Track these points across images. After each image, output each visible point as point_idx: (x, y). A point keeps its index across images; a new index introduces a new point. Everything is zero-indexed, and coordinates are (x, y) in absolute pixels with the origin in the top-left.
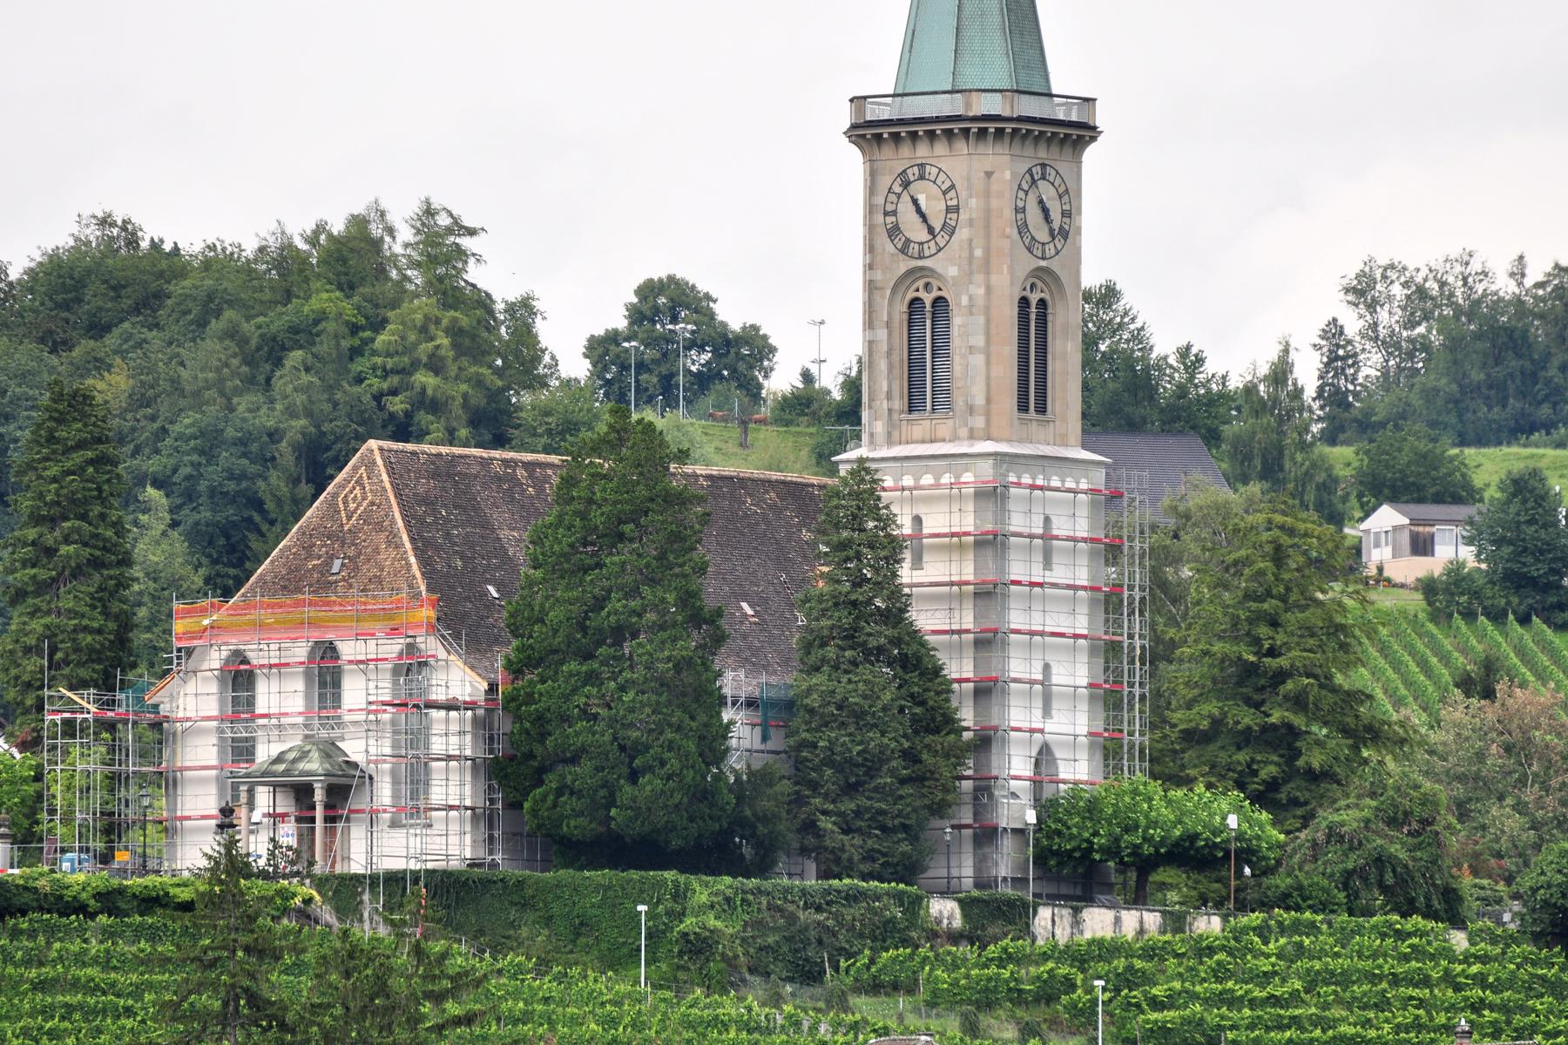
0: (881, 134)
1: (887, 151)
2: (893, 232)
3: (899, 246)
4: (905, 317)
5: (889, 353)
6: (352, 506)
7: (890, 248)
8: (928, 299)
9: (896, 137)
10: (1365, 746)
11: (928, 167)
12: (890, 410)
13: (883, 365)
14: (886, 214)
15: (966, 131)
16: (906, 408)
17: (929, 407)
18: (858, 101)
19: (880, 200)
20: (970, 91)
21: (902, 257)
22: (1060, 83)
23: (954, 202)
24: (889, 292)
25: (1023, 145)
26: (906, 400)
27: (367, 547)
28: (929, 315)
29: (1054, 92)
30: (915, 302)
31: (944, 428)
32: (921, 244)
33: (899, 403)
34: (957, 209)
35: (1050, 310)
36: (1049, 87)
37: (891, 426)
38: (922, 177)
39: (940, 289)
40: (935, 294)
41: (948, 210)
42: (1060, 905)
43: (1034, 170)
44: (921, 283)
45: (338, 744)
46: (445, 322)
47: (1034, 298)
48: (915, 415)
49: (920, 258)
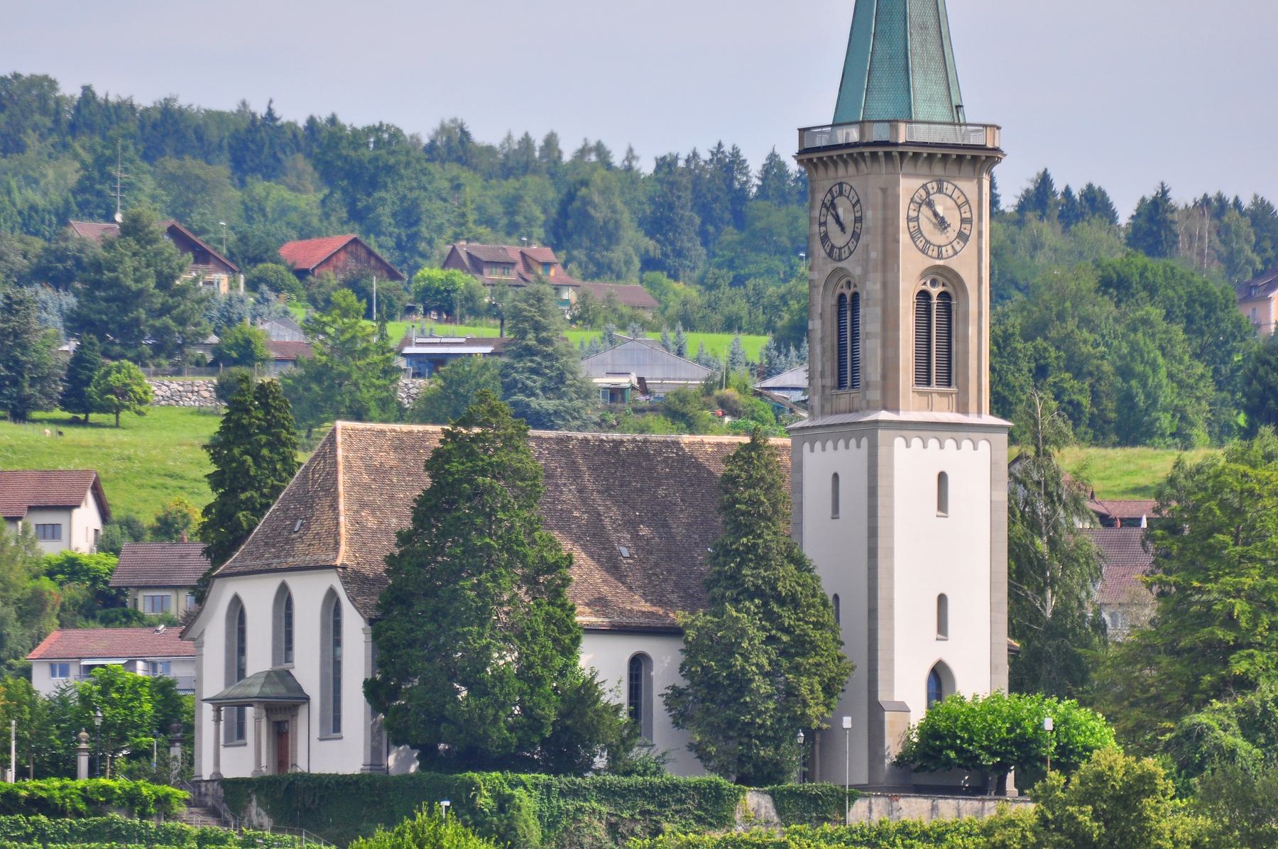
0: (877, 153)
4: (835, 309)
5: (822, 340)
8: (848, 293)
9: (874, 155)
12: (823, 387)
14: (821, 224)
15: (945, 157)
16: (836, 385)
17: (849, 383)
18: (802, 131)
22: (971, 114)
24: (821, 289)
25: (916, 166)
26: (836, 378)
30: (842, 296)
33: (830, 381)
35: (954, 302)
38: (841, 194)
40: (853, 290)
42: (876, 796)
46: (180, 328)
47: (935, 291)
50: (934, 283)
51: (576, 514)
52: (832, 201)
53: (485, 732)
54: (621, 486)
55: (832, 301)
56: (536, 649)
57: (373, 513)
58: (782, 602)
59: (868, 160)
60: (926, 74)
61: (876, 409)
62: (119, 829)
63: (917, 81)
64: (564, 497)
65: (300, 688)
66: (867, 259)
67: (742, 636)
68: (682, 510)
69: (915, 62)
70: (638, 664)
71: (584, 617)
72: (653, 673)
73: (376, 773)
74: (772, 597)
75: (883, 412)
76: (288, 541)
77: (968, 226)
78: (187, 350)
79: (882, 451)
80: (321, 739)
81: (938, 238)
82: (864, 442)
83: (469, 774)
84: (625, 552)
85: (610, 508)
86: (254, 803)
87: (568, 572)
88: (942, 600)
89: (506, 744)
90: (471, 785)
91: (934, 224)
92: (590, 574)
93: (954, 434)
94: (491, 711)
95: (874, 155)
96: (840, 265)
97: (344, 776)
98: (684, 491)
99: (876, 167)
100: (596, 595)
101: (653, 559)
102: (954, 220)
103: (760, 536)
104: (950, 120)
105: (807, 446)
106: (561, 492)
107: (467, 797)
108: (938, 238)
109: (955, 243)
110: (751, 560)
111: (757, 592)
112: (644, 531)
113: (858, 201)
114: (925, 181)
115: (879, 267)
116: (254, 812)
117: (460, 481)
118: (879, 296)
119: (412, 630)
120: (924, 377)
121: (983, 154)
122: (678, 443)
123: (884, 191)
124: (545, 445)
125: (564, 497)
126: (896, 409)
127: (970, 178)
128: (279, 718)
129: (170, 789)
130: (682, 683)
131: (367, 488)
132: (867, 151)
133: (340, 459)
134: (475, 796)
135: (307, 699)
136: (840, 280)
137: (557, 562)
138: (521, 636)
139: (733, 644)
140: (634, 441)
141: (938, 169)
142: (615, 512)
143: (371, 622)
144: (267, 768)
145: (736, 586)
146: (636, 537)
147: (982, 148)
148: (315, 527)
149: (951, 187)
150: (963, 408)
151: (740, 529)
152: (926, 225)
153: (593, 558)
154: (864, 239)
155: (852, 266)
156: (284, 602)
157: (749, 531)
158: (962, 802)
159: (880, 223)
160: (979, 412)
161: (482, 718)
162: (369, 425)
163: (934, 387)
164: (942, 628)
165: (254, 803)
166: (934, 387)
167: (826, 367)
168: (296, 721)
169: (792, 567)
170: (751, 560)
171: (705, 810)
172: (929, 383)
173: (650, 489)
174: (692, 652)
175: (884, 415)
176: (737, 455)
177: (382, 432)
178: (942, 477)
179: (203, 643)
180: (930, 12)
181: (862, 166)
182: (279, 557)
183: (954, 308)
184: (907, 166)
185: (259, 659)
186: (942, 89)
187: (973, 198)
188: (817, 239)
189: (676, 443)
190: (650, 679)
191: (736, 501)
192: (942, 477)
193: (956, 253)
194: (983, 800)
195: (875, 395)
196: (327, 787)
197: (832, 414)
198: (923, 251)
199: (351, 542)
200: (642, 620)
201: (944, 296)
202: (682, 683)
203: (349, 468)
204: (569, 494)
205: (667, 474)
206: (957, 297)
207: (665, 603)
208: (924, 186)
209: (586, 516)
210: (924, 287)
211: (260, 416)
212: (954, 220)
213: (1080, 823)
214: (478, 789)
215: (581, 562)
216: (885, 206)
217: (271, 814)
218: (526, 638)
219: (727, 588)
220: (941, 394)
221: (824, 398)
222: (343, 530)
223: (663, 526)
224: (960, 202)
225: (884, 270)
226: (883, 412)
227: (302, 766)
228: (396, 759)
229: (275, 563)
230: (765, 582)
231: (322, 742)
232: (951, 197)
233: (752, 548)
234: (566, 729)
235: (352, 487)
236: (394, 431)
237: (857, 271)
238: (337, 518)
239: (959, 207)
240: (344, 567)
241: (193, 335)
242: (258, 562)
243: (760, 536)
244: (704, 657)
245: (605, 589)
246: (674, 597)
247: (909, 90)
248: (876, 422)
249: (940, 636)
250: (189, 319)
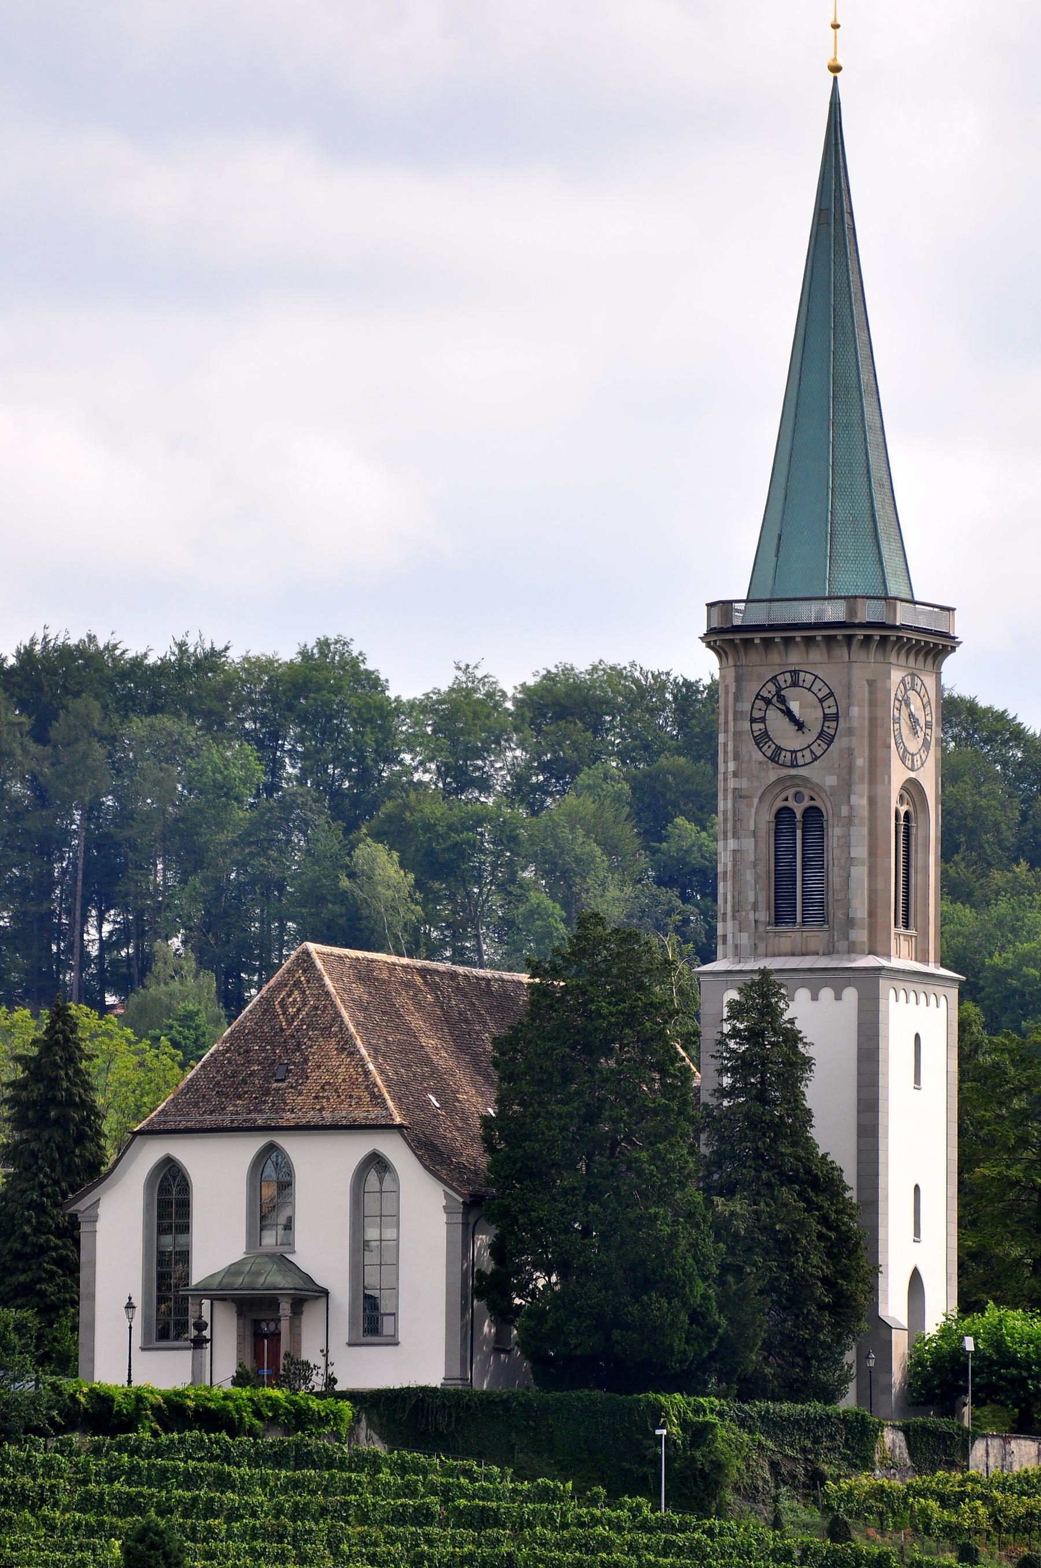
1: (754, 657)
2: (762, 739)
3: (769, 754)
5: (755, 864)
6: (292, 1010)
7: (758, 756)
8: (799, 809)
11: (802, 674)
13: (749, 876)
14: (753, 720)
16: (773, 921)
17: (799, 919)
19: (746, 706)
20: (855, 597)
21: (771, 764)
23: (833, 710)
24: (756, 801)
26: (773, 911)
27: (314, 1054)
28: (799, 825)
29: (917, 599)
31: (816, 937)
32: (794, 752)
34: (836, 717)
36: (887, 593)
37: (757, 938)
38: (795, 684)
39: (812, 799)
40: (807, 803)
41: (826, 718)
43: (780, 678)
44: (790, 793)
45: (287, 1256)
48: (783, 928)
49: (794, 765)
55: (768, 816)
62: (310, 1452)
66: (850, 768)
75: (870, 957)
80: (143, 1349)
88: (917, 1188)
95: (868, 638)
109: (814, 747)
115: (866, 779)
118: (866, 813)
123: (871, 683)
126: (888, 955)
149: (809, 678)
154: (840, 743)
167: (760, 897)
168: (300, 1319)
171: (851, 1449)
179: (97, 1216)
195: (860, 935)
197: (766, 956)
206: (916, 818)
210: (786, 804)
221: (757, 937)
231: (352, 1348)
232: (809, 689)
247: (881, 564)
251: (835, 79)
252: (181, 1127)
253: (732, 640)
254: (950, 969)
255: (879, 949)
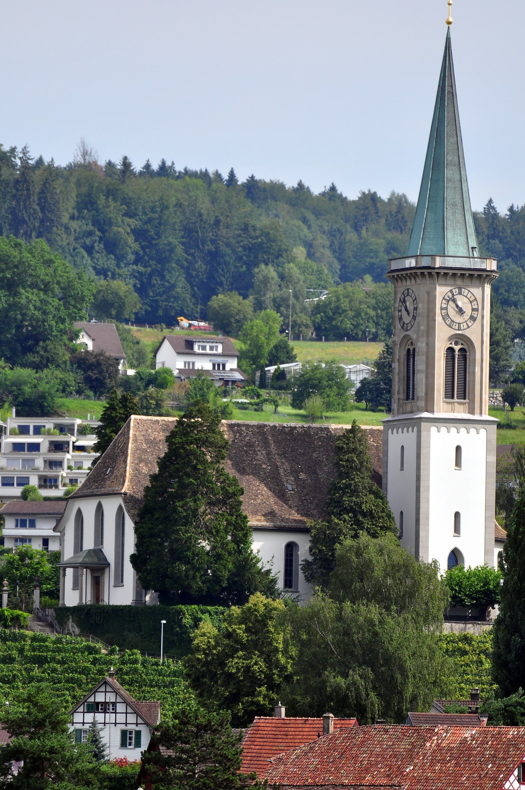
4: (405, 357)
5: (399, 373)
8: (411, 348)
10: (141, 264)
12: (399, 399)
25: (446, 279)
33: (402, 396)
35: (468, 354)
38: (408, 295)
40: (413, 347)
47: (457, 348)
50: (456, 343)
51: (264, 466)
52: (404, 299)
53: (188, 584)
54: (292, 452)
55: (404, 353)
56: (218, 539)
57: (146, 465)
58: (365, 515)
59: (420, 277)
60: (454, 230)
61: (422, 411)
63: (449, 234)
64: (258, 457)
65: (106, 559)
66: (419, 330)
67: (340, 533)
68: (325, 466)
69: (448, 224)
70: (290, 548)
71: (253, 522)
72: (299, 553)
73: (139, 605)
74: (360, 512)
76: (104, 480)
77: (476, 313)
78: (500, 375)
79: (423, 434)
80: (115, 586)
81: (458, 319)
82: (415, 429)
83: (180, 606)
84: (290, 487)
85: (284, 464)
86: (71, 620)
87: (241, 498)
88: (457, 515)
89: (200, 590)
90: (181, 611)
91: (456, 312)
92: (268, 499)
93: (466, 425)
94: (191, 572)
96: (407, 333)
97: (116, 606)
98: (329, 455)
99: (424, 281)
100: (270, 511)
101: (305, 491)
102: (468, 310)
103: (353, 479)
104: (467, 255)
105: (390, 431)
106: (257, 455)
107: (178, 619)
108: (458, 319)
109: (468, 322)
110: (348, 493)
111: (351, 510)
112: (302, 476)
113: (416, 299)
114: (451, 288)
116: (70, 625)
117: (179, 448)
119: (152, 528)
120: (449, 394)
121: (484, 274)
122: (328, 429)
123: (428, 293)
124: (250, 429)
125: (258, 457)
126: (432, 412)
127: (478, 287)
128: (97, 574)
129: (20, 612)
130: (310, 559)
131: (144, 451)
132: (419, 271)
133: (131, 435)
134: (182, 618)
135: (109, 565)
136: (408, 341)
137: (234, 492)
138: (210, 532)
139: (334, 537)
140: (303, 427)
141: (459, 282)
142: (287, 466)
143: (136, 523)
144: (88, 599)
145: (340, 506)
146: (297, 479)
147: (484, 270)
148: (116, 472)
149: (466, 292)
150: (472, 411)
151: (341, 476)
152: (452, 311)
153: (271, 490)
155: (411, 333)
156: (100, 511)
157: (347, 475)
158: (454, 624)
159: (426, 311)
160: (481, 413)
161: (187, 576)
162: (149, 418)
163: (456, 400)
164: (457, 530)
165: (71, 620)
166: (456, 400)
169: (372, 496)
170: (348, 493)
172: (453, 398)
173: (308, 453)
174: (315, 541)
175: (425, 415)
176: (344, 436)
177: (157, 421)
178: (458, 449)
180: (458, 197)
181: (418, 280)
182: (98, 488)
183: (468, 357)
184: (442, 280)
185: (89, 544)
186: (464, 238)
187: (479, 297)
188: (397, 319)
189: (327, 429)
190: (297, 556)
191: (341, 460)
192: (458, 449)
193: (469, 327)
194: (466, 624)
195: (421, 404)
196: (107, 612)
198: (449, 326)
199: (131, 480)
200: (293, 524)
201: (462, 350)
202: (310, 559)
203: (135, 440)
204: (261, 456)
205: (320, 445)
207: (309, 515)
208: (451, 291)
209: (269, 468)
210: (451, 346)
211: (122, 412)
212: (468, 310)
213: (237, 634)
214: (184, 614)
215: (264, 492)
216: (428, 302)
217: (79, 626)
218: (212, 533)
219: (335, 507)
220: (460, 403)
222: (128, 474)
223: (313, 473)
224: (471, 300)
225: (428, 336)
226: (426, 413)
227: (106, 602)
228: (150, 598)
229: (96, 491)
230: (356, 505)
232: (466, 297)
233: (348, 486)
234: (235, 583)
235: (136, 451)
236: (164, 421)
237: (414, 337)
238: (126, 468)
239: (471, 302)
240: (125, 494)
241: (504, 366)
242: (89, 491)
243: (353, 479)
244: (321, 544)
245: (275, 507)
246: (315, 512)
248: (421, 418)
249: (456, 535)
250: (500, 357)
251: (449, 27)
252: (99, 493)
253: (393, 276)
254: (494, 417)
255: (429, 410)
